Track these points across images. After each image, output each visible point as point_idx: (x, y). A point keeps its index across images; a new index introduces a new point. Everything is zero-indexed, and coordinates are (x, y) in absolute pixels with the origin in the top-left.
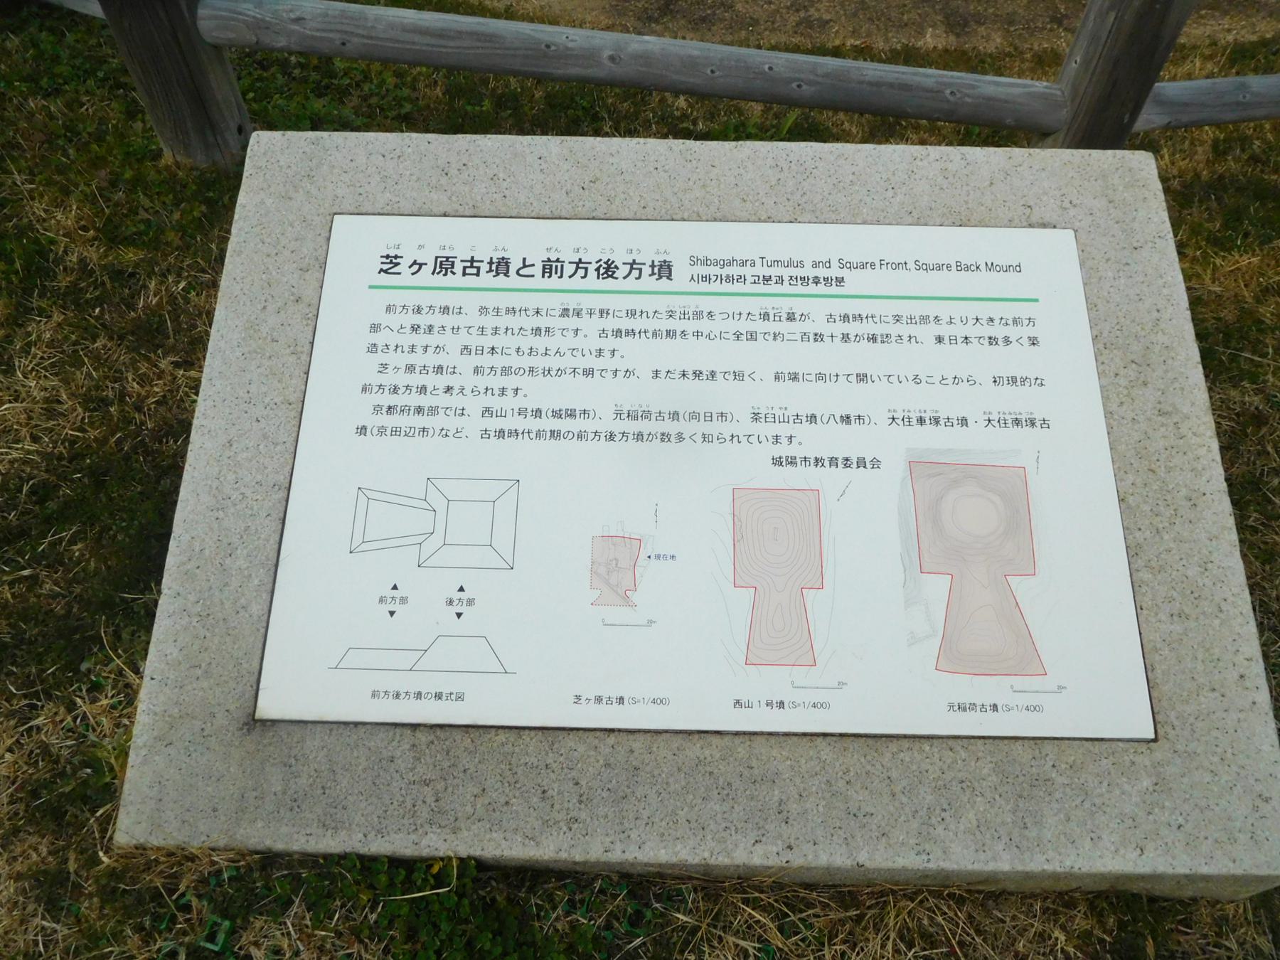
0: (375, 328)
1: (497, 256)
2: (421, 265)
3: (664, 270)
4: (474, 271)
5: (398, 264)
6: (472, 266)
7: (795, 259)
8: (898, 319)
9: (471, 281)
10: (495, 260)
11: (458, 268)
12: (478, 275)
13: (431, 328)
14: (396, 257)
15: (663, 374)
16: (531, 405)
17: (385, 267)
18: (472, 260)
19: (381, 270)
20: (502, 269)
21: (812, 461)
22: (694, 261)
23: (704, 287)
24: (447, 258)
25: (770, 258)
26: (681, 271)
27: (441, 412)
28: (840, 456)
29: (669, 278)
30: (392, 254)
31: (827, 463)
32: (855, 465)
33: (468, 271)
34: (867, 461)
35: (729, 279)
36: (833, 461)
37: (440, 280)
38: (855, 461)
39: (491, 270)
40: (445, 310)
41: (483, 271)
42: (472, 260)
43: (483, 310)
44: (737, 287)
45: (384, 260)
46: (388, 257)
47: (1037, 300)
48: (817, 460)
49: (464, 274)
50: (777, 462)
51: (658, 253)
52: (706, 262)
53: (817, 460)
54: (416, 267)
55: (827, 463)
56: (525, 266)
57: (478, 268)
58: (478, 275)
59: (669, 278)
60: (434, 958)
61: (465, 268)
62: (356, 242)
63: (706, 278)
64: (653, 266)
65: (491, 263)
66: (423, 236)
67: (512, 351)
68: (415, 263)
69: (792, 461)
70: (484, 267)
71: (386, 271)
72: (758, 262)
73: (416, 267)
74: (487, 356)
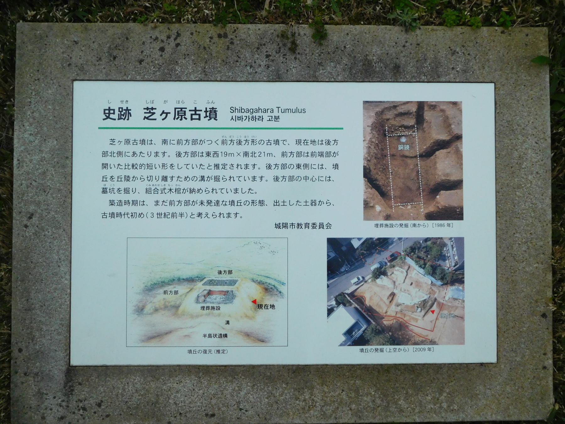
0: (105, 154)
1: (209, 106)
2: (167, 114)
3: (212, 113)
4: (197, 117)
5: (154, 113)
6: (196, 114)
7: (300, 108)
8: (127, 142)
9: (196, 123)
10: (208, 110)
11: (188, 115)
12: (199, 119)
14: (152, 109)
16: (257, 198)
17: (147, 115)
18: (195, 110)
19: (145, 118)
20: (213, 115)
21: (296, 225)
22: (233, 110)
23: (239, 124)
24: (181, 109)
25: (283, 107)
26: (224, 116)
28: (303, 222)
29: (215, 119)
31: (303, 227)
32: (318, 227)
33: (194, 117)
34: (325, 224)
35: (254, 119)
36: (307, 225)
37: (178, 123)
38: (318, 225)
39: (206, 116)
40: (143, 142)
41: (202, 117)
42: (195, 110)
43: (299, 142)
44: (258, 124)
45: (146, 111)
46: (147, 109)
47: (342, 129)
49: (192, 119)
50: (329, 226)
51: (209, 103)
52: (241, 110)
54: (164, 115)
55: (303, 227)
57: (199, 115)
58: (199, 119)
59: (215, 119)
61: (192, 115)
63: (240, 118)
65: (206, 111)
66: (136, 94)
68: (163, 112)
70: (203, 114)
71: (147, 118)
72: (276, 110)
73: (164, 115)
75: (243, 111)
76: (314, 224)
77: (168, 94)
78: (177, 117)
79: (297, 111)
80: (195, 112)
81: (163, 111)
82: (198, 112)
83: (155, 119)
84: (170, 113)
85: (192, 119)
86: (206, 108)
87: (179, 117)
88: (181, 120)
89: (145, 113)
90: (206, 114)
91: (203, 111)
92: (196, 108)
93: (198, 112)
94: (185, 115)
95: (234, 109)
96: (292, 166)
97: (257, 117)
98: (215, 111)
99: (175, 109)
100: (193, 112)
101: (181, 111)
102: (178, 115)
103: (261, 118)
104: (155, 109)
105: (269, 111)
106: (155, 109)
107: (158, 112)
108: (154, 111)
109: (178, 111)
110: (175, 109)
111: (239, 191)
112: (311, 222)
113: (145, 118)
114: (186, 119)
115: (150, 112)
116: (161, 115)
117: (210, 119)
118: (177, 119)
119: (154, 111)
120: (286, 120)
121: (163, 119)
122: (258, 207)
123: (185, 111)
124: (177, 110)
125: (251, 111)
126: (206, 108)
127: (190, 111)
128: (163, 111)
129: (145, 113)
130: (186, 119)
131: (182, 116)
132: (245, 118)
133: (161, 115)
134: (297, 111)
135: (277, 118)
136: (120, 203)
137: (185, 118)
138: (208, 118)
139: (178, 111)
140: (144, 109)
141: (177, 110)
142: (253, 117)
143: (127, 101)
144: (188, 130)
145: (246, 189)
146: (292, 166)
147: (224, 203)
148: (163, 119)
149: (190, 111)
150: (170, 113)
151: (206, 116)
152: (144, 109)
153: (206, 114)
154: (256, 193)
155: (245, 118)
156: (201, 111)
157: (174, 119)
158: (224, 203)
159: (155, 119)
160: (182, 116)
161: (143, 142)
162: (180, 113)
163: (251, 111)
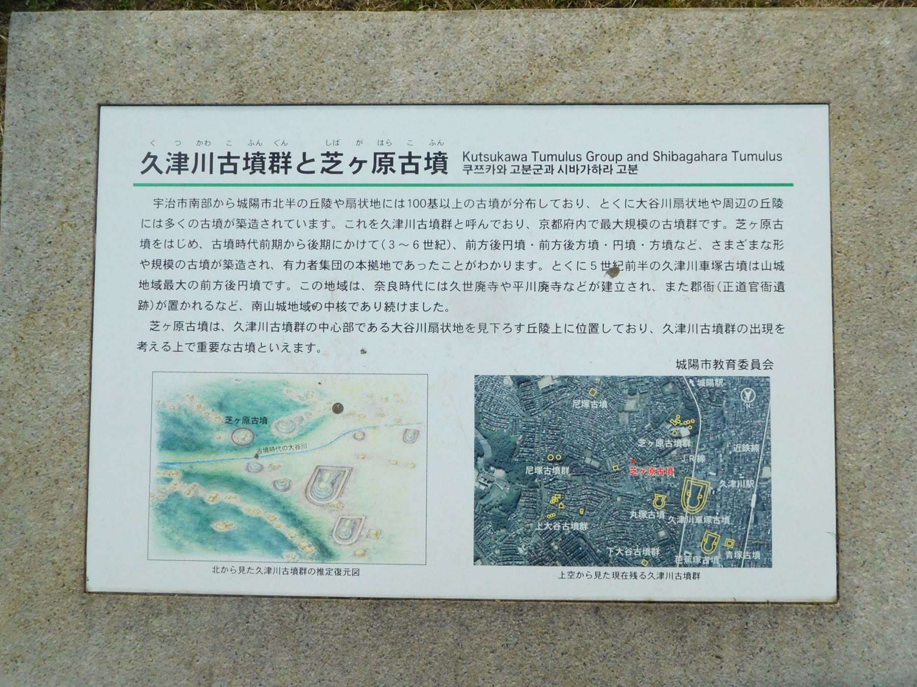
1: (433, 150)
2: (361, 162)
4: (231, 168)
5: (338, 162)
6: (410, 163)
10: (250, 156)
13: (729, 244)
14: (336, 154)
15: (676, 287)
17: (327, 165)
18: (410, 157)
20: (440, 165)
21: (712, 363)
24: (386, 154)
25: (743, 151)
26: (455, 164)
27: (356, 327)
30: (332, 152)
33: (226, 168)
34: (761, 362)
37: (379, 178)
38: (750, 363)
42: (410, 157)
44: (604, 178)
45: (325, 158)
46: (328, 154)
48: (716, 362)
49: (404, 172)
51: (252, 144)
53: (716, 362)
54: (356, 165)
56: (305, 162)
57: (235, 165)
60: (345, 686)
61: (403, 165)
62: (127, 134)
64: (247, 159)
65: (247, 159)
67: (588, 266)
68: (355, 160)
69: (214, 347)
71: (327, 170)
73: (356, 165)
74: (186, 280)
75: (675, 157)
76: (743, 362)
77: (359, 129)
78: (378, 168)
79: (767, 157)
80: (410, 161)
81: (355, 158)
82: (413, 161)
83: (341, 173)
84: (366, 162)
85: (222, 172)
86: (428, 154)
87: (381, 169)
88: (385, 173)
89: (324, 161)
90: (428, 163)
91: (423, 158)
92: (410, 153)
93: (232, 161)
94: (392, 165)
95: (660, 155)
96: (319, 285)
97: (602, 168)
98: (444, 158)
99: (375, 154)
100: (225, 161)
101: (386, 157)
102: (380, 165)
103: (502, 170)
104: (342, 155)
105: (719, 157)
106: (342, 155)
107: (346, 160)
108: (339, 158)
109: (380, 159)
110: (375, 154)
111: (420, 307)
112: (738, 358)
113: (324, 170)
114: (394, 171)
115: (332, 161)
116: (351, 165)
117: (254, 171)
118: (378, 172)
119: (339, 158)
120: (648, 171)
121: (354, 173)
122: (774, 295)
123: (392, 159)
124: (378, 156)
125: (689, 157)
126: (428, 154)
127: (400, 157)
128: (355, 158)
129: (324, 161)
130: (394, 171)
131: (386, 166)
132: (581, 169)
133: (351, 165)
134: (767, 157)
135: (633, 169)
136: (393, 286)
137: (391, 169)
138: (432, 170)
139: (380, 159)
140: (322, 155)
141: (378, 156)
142: (595, 167)
143: (359, 142)
144: (395, 187)
145: (430, 304)
146: (319, 285)
147: (226, 347)
148: (354, 173)
149: (400, 157)
150: (366, 162)
151: (429, 167)
152: (322, 155)
153: (428, 163)
154: (447, 310)
155: (581, 169)
156: (238, 157)
157: (373, 172)
158: (226, 347)
159: (341, 173)
160: (386, 166)
161: (375, 203)
162: (383, 162)
163: (689, 157)
